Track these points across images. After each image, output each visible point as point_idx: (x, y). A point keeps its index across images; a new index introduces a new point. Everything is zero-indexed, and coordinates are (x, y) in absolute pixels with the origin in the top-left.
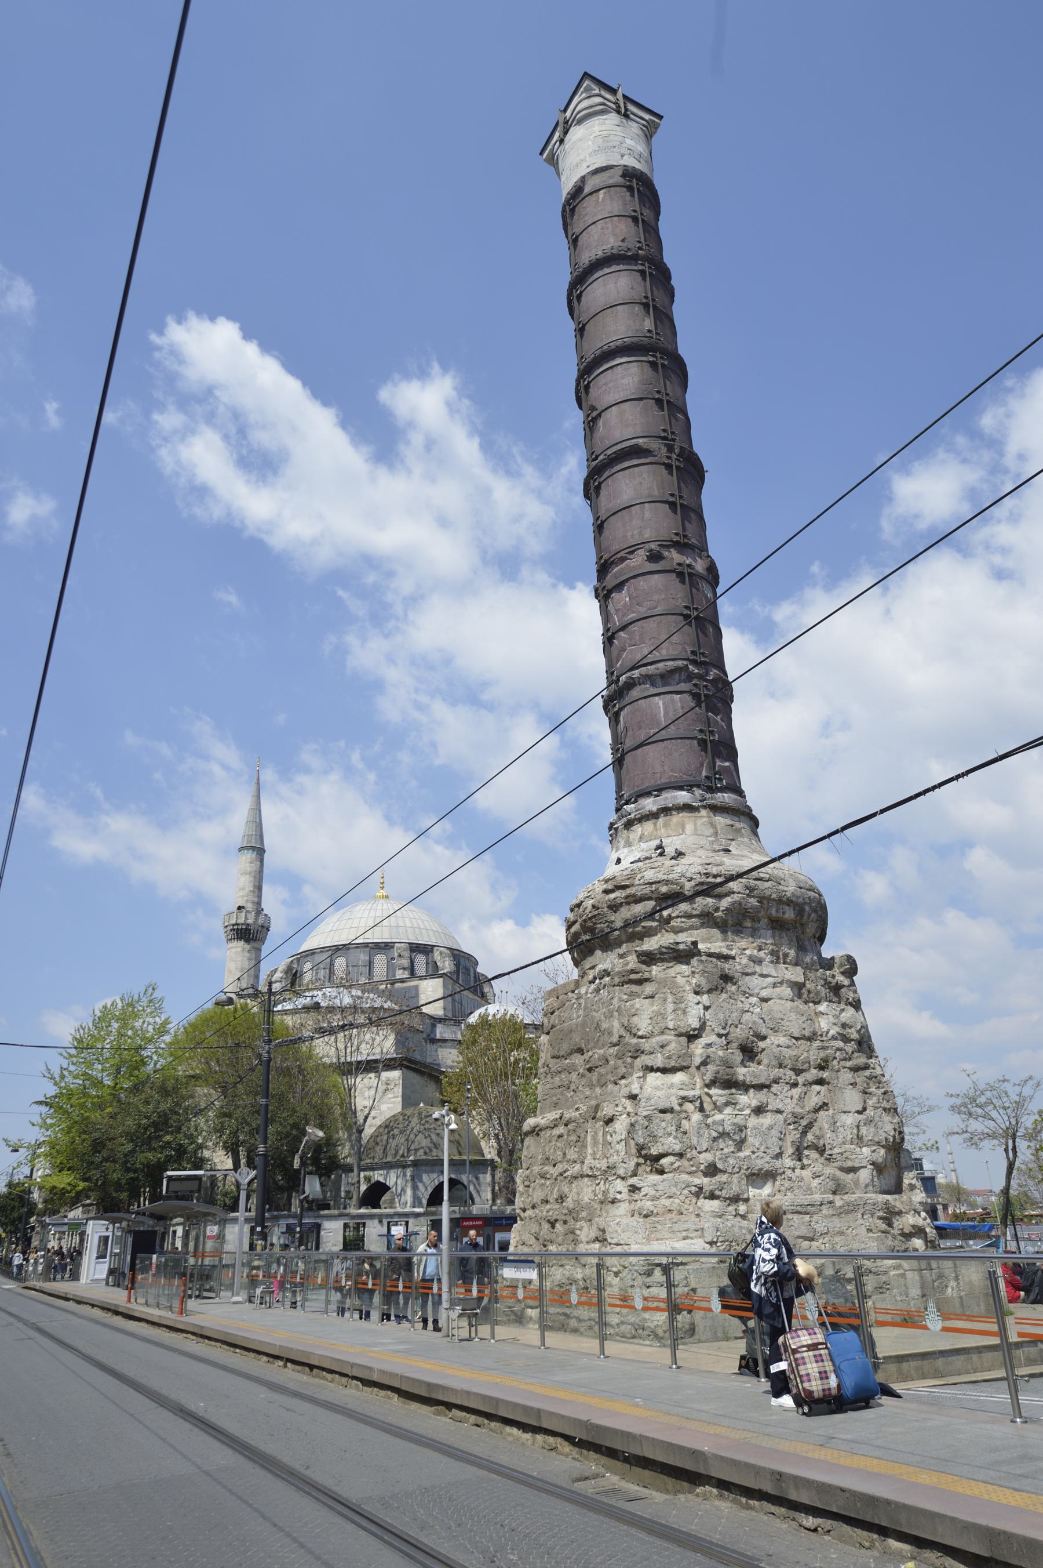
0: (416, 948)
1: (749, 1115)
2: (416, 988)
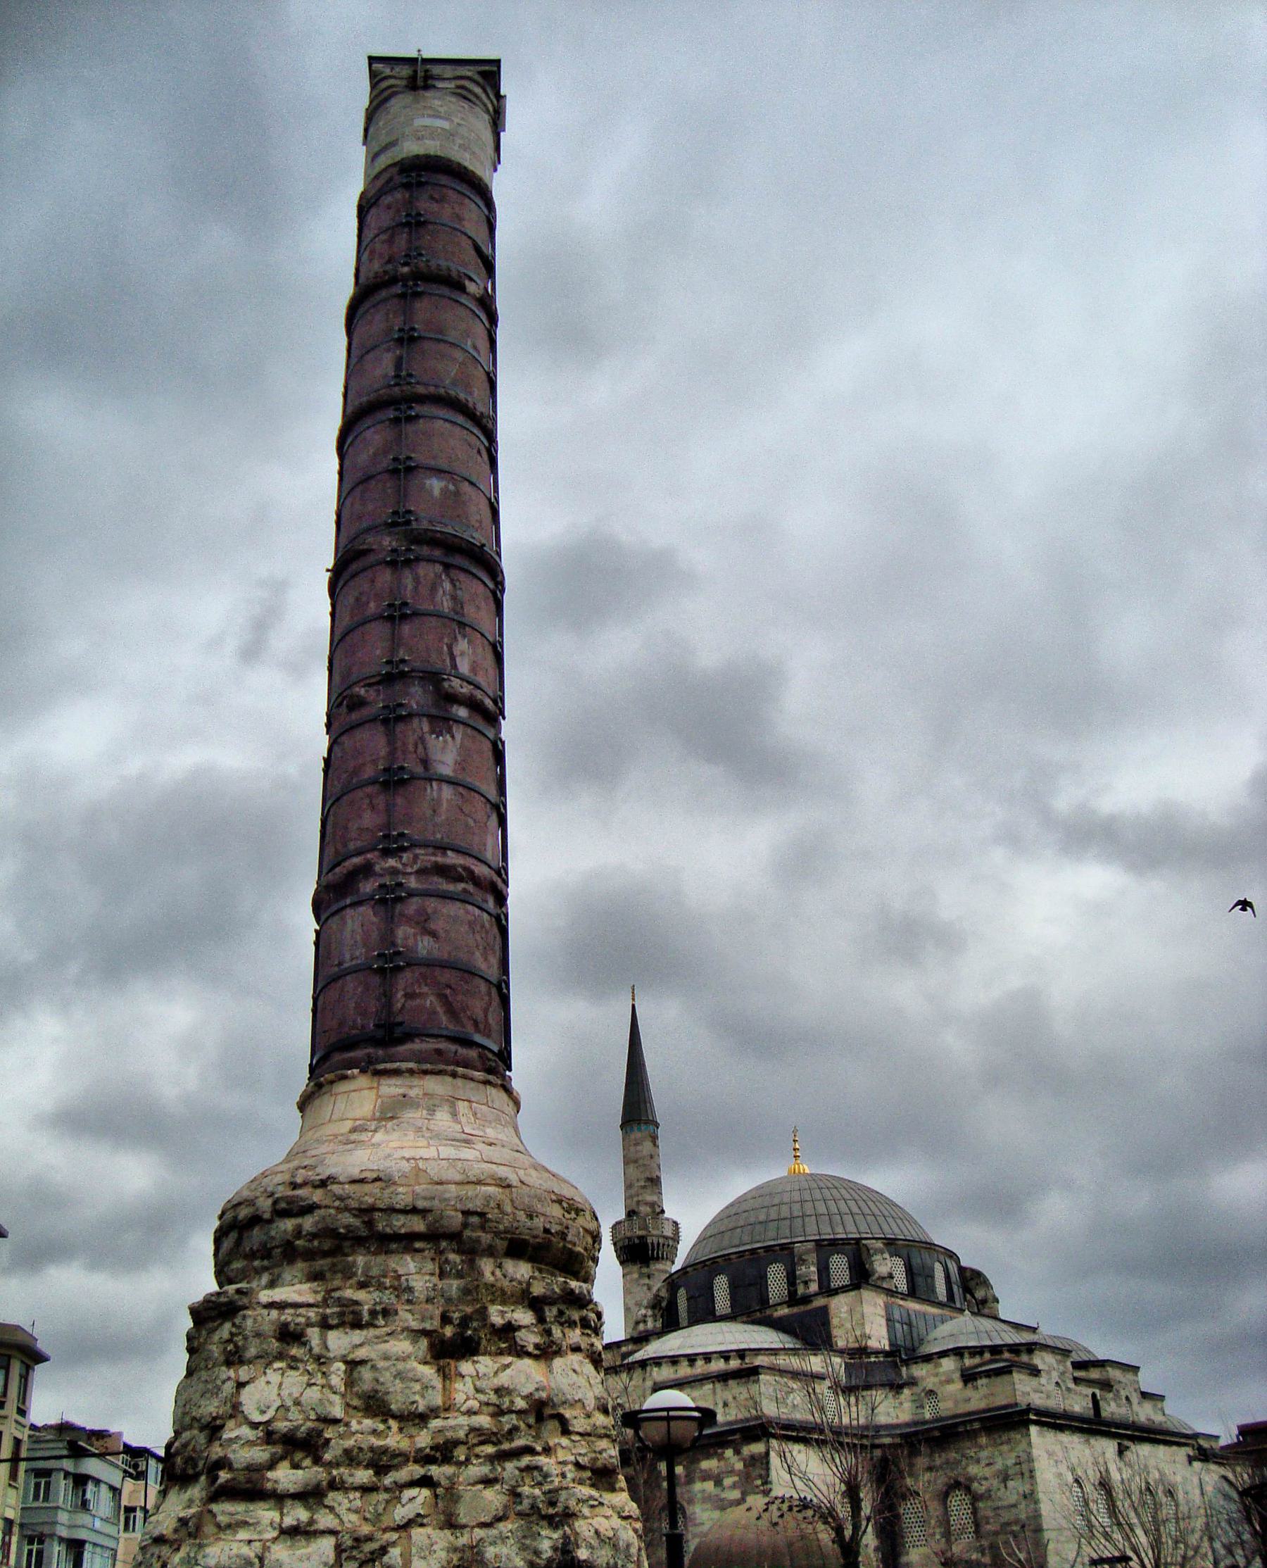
0: (826, 1247)
1: (275, 1540)
2: (824, 1310)
